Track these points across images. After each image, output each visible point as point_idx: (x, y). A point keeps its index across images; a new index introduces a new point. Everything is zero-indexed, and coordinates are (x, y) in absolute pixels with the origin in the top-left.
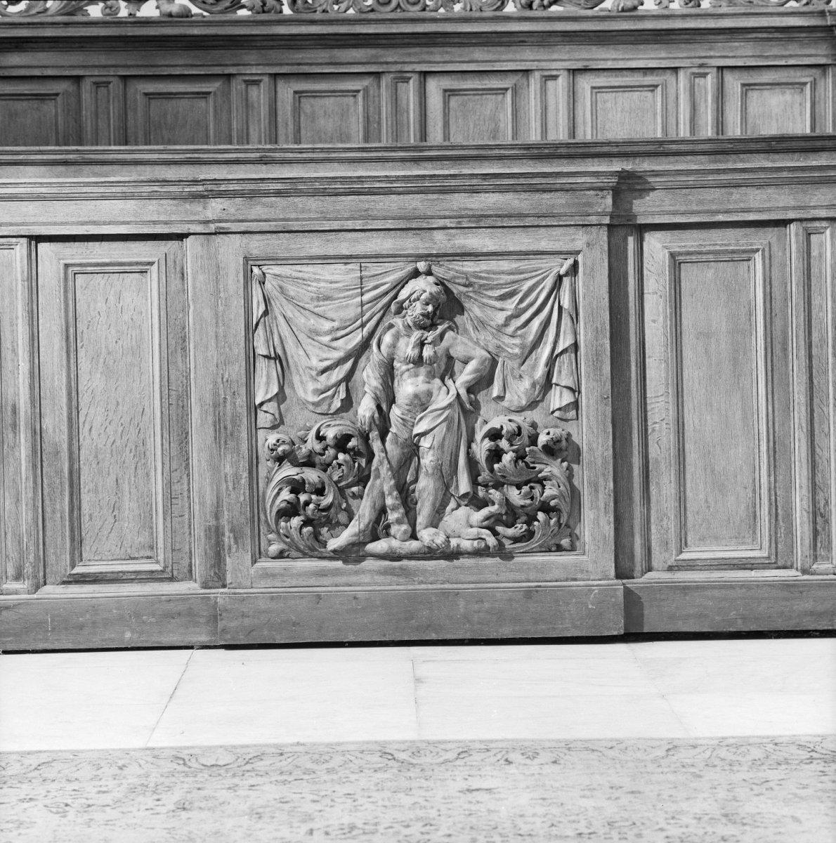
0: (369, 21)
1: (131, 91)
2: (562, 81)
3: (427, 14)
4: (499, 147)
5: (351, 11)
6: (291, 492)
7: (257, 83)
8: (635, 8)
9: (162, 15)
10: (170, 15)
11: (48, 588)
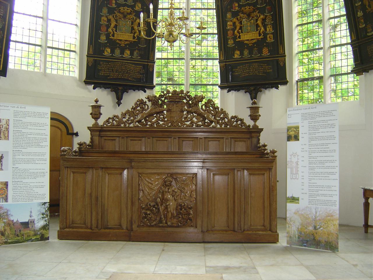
0: (169, 128)
1: (128, 139)
2: (229, 139)
3: (180, 127)
4: (169, 152)
5: (166, 126)
6: (145, 214)
7: (176, 138)
8: (216, 127)
9: (134, 126)
10: (135, 126)
11: (102, 230)
